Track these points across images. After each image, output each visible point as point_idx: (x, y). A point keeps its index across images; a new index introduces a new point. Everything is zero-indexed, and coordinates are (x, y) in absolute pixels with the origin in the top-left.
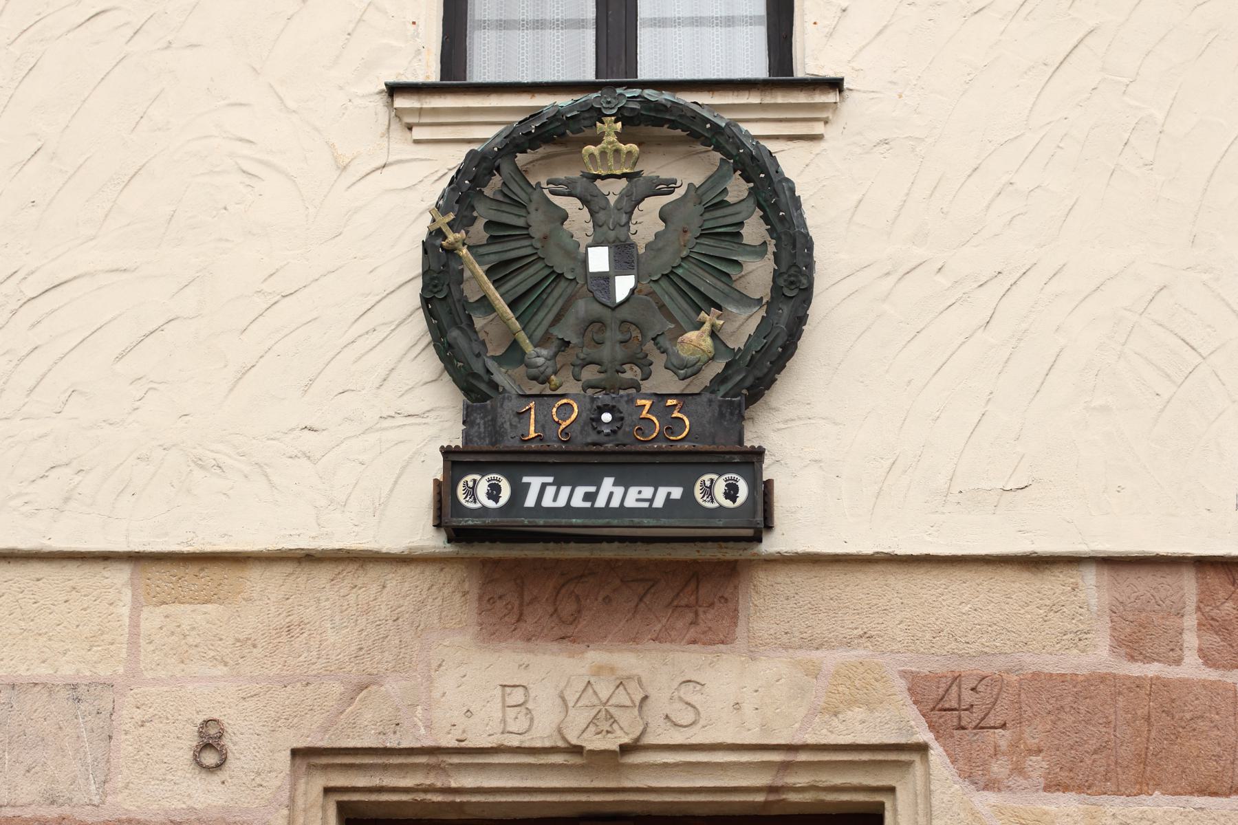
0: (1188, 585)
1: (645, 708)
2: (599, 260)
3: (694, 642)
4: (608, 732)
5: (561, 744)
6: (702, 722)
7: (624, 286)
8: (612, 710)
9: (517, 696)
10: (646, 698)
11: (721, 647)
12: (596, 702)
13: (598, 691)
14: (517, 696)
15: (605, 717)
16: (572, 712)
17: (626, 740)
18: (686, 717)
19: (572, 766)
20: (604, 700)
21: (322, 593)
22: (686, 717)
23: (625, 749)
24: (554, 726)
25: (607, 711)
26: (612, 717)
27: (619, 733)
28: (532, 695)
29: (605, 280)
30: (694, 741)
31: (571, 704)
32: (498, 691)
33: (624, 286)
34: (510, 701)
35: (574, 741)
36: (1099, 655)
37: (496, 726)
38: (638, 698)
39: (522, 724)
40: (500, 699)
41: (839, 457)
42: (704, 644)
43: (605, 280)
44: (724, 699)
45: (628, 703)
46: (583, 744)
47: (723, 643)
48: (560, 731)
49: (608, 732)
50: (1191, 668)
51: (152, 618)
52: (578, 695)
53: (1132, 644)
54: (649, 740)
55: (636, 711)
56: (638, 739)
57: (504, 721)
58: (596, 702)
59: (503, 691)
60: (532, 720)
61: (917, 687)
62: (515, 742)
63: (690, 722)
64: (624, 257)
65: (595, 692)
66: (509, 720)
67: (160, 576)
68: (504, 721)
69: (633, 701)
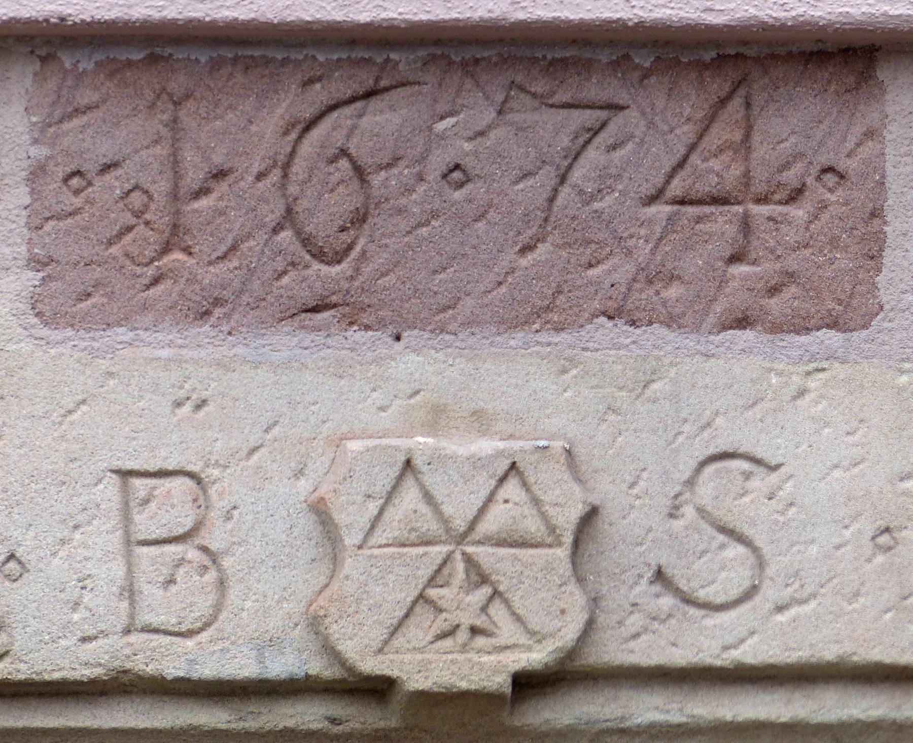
1: (590, 548)
3: (742, 322)
4: (475, 631)
5: (318, 667)
6: (770, 593)
8: (483, 554)
9: (171, 507)
10: (591, 515)
11: (830, 338)
12: (431, 526)
13: (439, 494)
14: (171, 507)
15: (463, 557)
16: (350, 565)
17: (536, 657)
18: (726, 570)
19: (302, 45)
20: (460, 524)
22: (726, 570)
23: (528, 684)
24: (294, 607)
25: (469, 560)
26: (484, 580)
27: (507, 631)
28: (220, 505)
30: (752, 653)
31: (351, 539)
32: (110, 488)
34: (147, 524)
35: (371, 665)
37: (104, 604)
38: (568, 517)
39: (191, 597)
40: (115, 520)
42: (776, 329)
45: (533, 526)
46: (395, 673)
47: (834, 325)
48: (315, 624)
49: (475, 631)
52: (373, 507)
54: (613, 651)
55: (562, 553)
56: (572, 653)
57: (130, 592)
58: (431, 526)
59: (125, 490)
60: (222, 584)
62: (173, 661)
63: (734, 593)
65: (428, 497)
66: (151, 593)
68: (130, 592)
69: (552, 529)
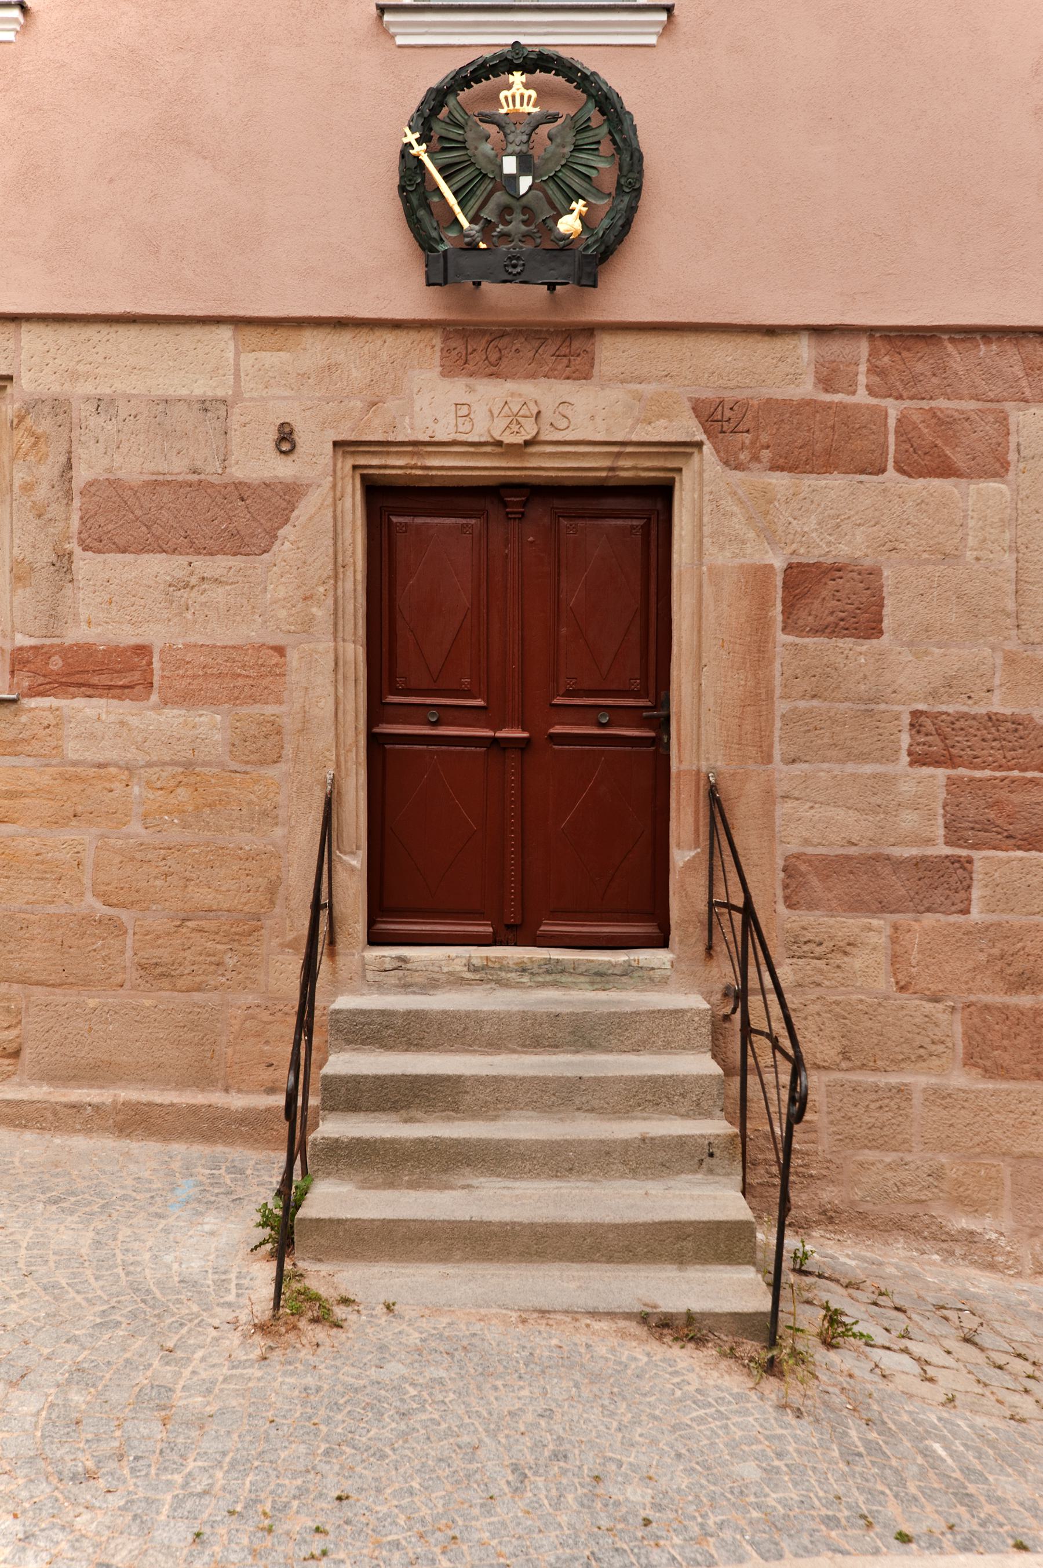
0: (863, 347)
2: (510, 165)
7: (525, 183)
15: (515, 420)
21: (343, 347)
29: (513, 179)
33: (525, 183)
36: (806, 389)
41: (661, 272)
43: (513, 179)
44: (577, 419)
50: (862, 397)
51: (248, 360)
53: (827, 382)
61: (698, 408)
64: (525, 164)
67: (251, 335)
